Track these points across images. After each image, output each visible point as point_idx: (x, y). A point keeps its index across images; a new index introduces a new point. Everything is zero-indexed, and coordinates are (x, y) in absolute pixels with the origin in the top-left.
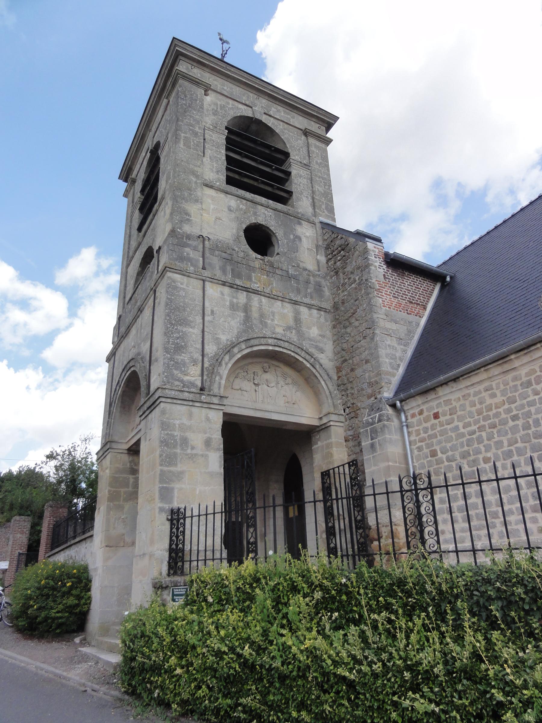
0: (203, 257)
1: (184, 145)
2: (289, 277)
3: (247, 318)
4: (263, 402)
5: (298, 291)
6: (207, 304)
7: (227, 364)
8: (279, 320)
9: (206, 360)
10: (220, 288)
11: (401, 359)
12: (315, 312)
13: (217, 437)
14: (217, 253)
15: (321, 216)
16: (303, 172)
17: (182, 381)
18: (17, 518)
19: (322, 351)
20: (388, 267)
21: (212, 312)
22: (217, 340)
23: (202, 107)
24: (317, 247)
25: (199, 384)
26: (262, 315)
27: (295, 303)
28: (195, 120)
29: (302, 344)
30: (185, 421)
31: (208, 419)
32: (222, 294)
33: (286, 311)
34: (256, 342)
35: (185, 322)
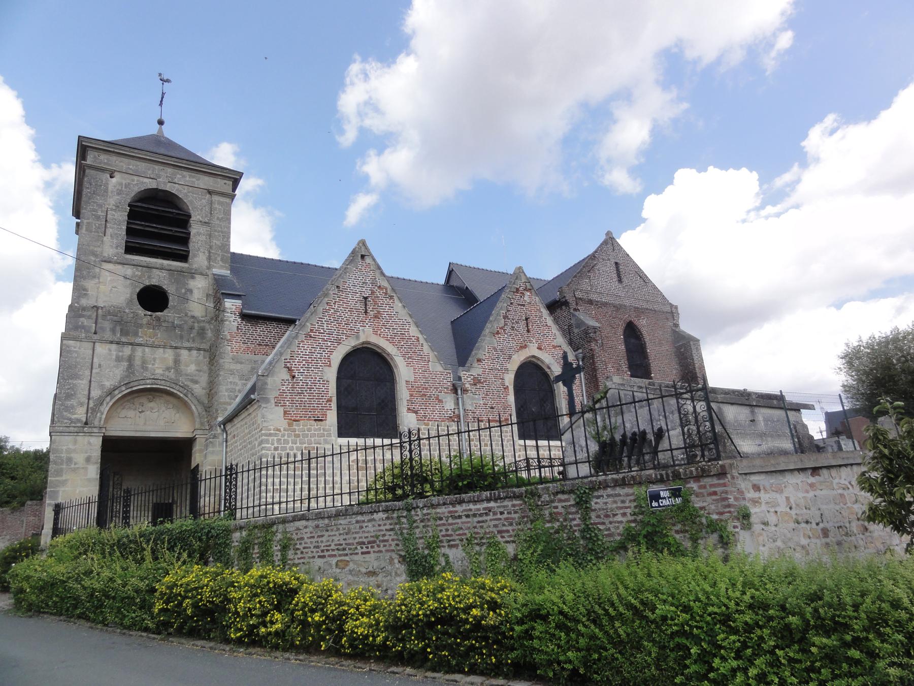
0: (96, 323)
1: (87, 230)
2: (174, 327)
3: (131, 366)
4: (145, 424)
5: (181, 337)
6: (95, 360)
7: (108, 403)
8: (158, 363)
9: (91, 402)
10: (108, 346)
11: (240, 391)
12: (194, 352)
13: (96, 453)
14: (109, 317)
15: (215, 267)
16: (203, 229)
17: (70, 419)
18: (29, 502)
19: (196, 382)
20: (243, 319)
21: (100, 366)
22: (102, 386)
23: (106, 191)
24: (208, 296)
25: (84, 420)
26: (144, 362)
27: (176, 348)
28: (98, 205)
29: (178, 380)
30: (71, 446)
31: (89, 443)
32: (110, 350)
33: (166, 355)
34: (136, 383)
35: (76, 376)
